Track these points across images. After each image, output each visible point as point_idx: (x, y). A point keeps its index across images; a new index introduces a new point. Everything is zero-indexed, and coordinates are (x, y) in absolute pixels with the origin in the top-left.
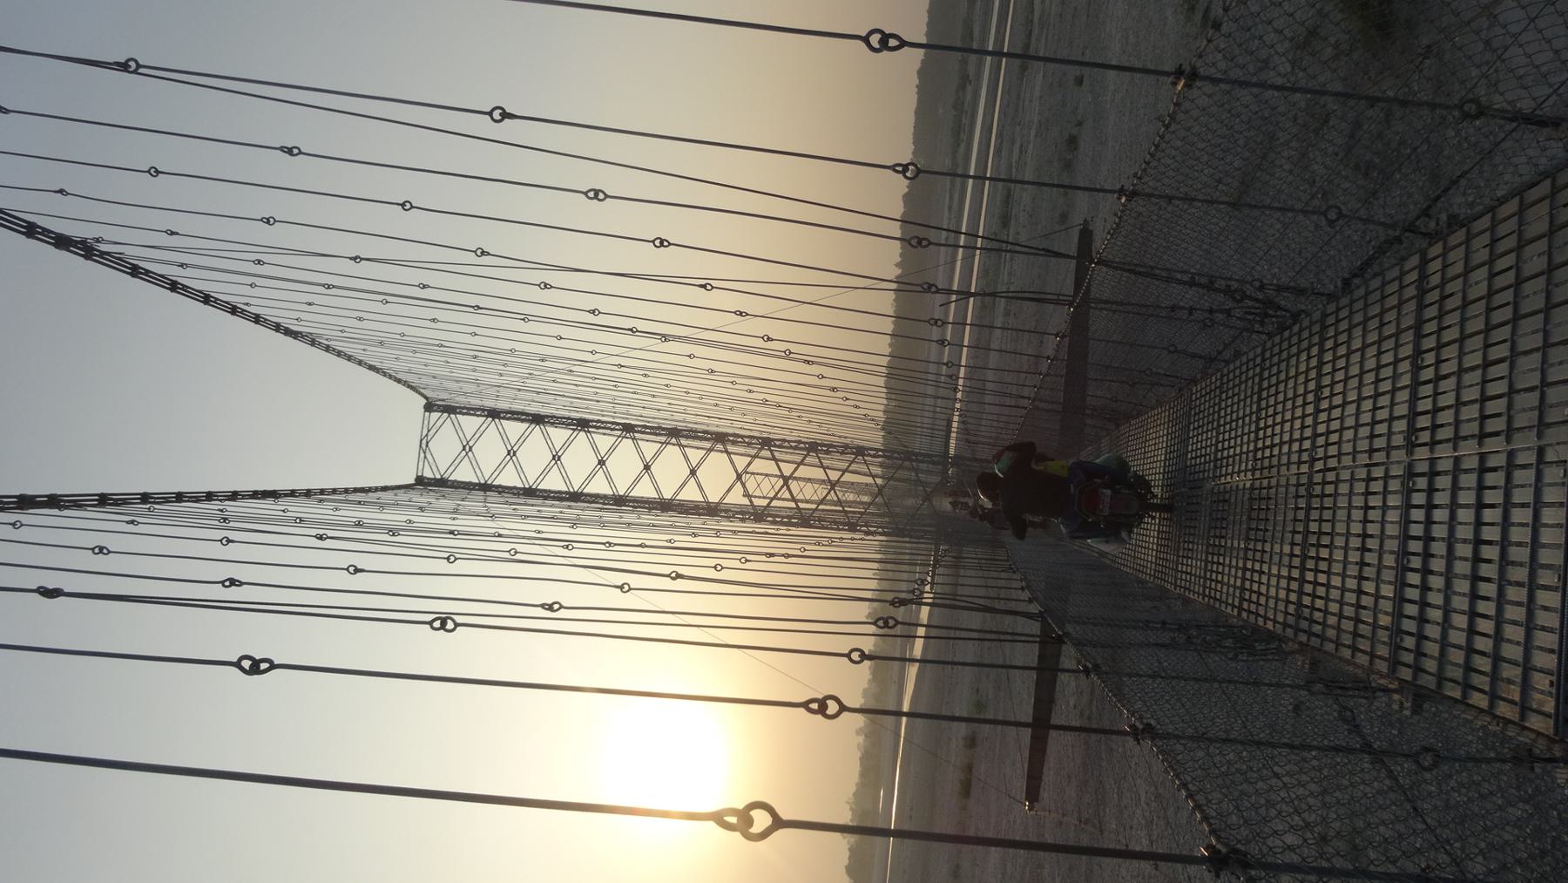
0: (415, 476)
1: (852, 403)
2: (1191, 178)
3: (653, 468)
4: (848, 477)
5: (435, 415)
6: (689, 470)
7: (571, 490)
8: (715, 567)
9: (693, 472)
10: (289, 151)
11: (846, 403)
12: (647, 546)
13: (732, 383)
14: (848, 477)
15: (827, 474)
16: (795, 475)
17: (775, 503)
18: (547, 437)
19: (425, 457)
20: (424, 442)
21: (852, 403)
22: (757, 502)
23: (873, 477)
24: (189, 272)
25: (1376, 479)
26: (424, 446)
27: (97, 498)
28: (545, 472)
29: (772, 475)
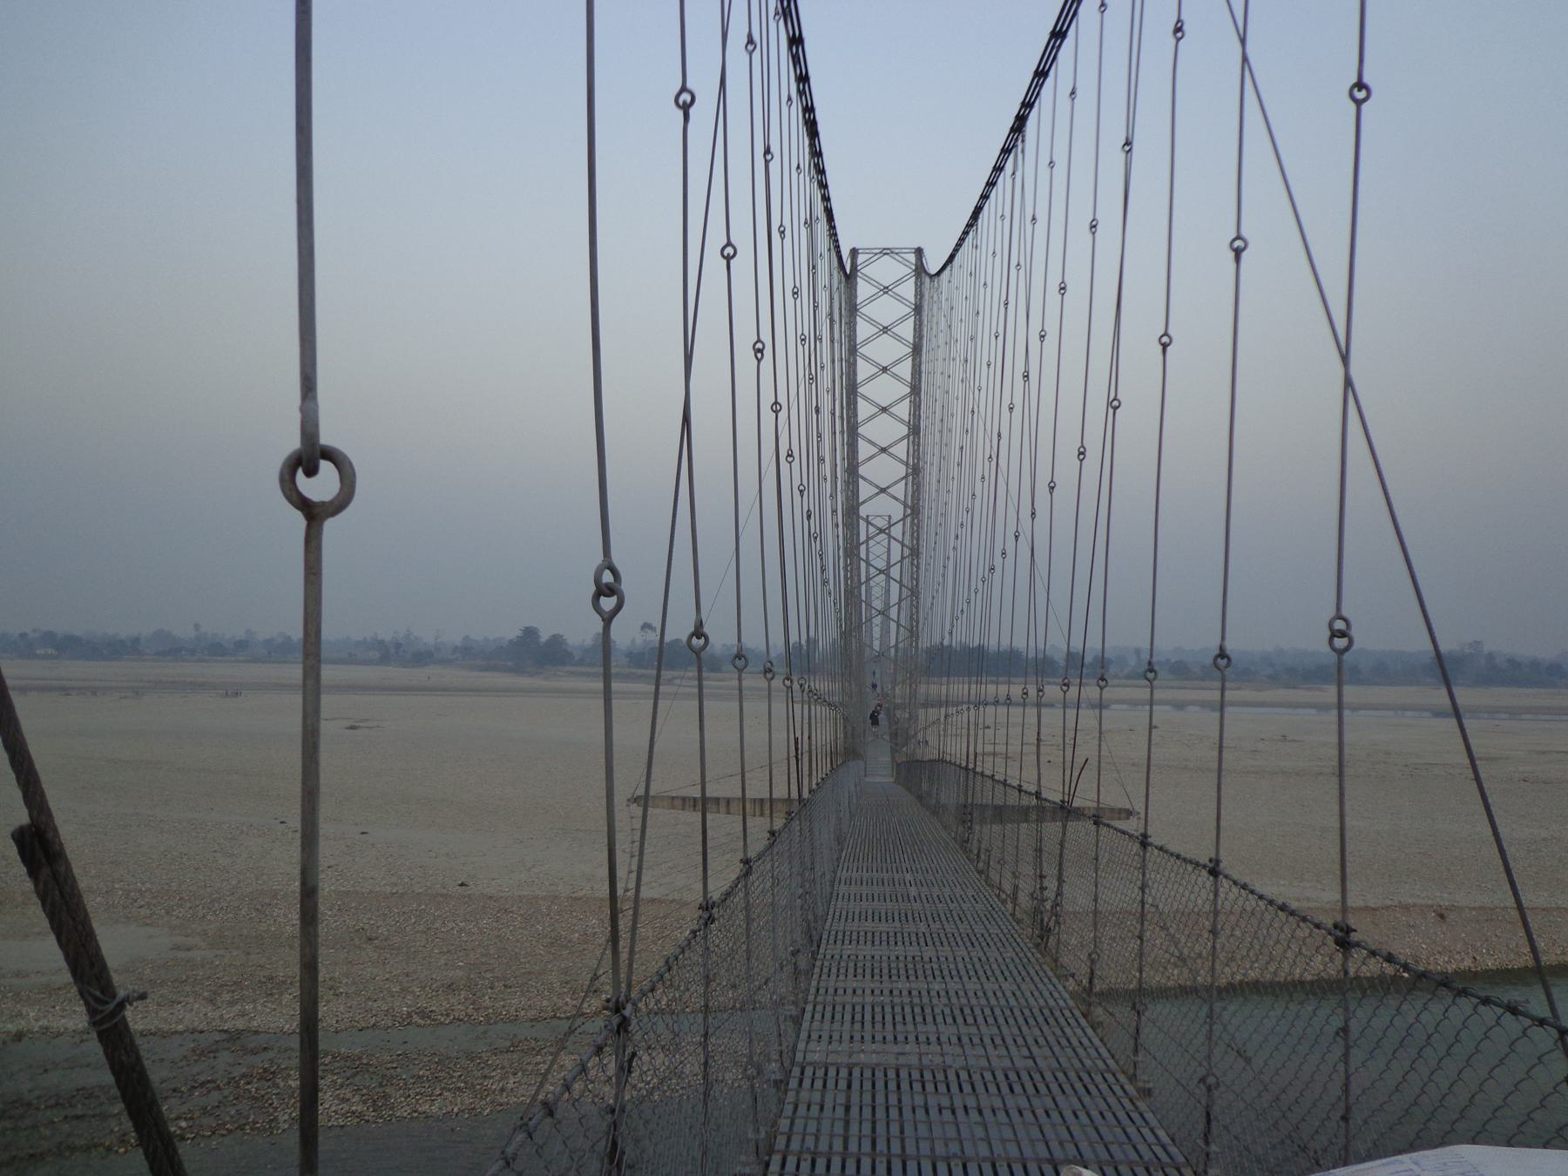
0: (857, 248)
1: (980, 588)
2: (1259, 924)
3: (883, 446)
4: (893, 626)
5: (912, 258)
6: (883, 375)
7: (858, 347)
8: (776, 403)
9: (883, 450)
10: (1178, 29)
11: (979, 580)
12: (767, 163)
13: (1018, 265)
14: (893, 626)
15: (895, 564)
16: (898, 580)
17: (863, 565)
18: (903, 319)
19: (876, 254)
20: (888, 251)
21: (980, 588)
22: (863, 548)
23: (896, 646)
24: (1009, 181)
25: (802, 1117)
26: (885, 251)
27: (810, 105)
28: (872, 322)
29: (889, 555)
